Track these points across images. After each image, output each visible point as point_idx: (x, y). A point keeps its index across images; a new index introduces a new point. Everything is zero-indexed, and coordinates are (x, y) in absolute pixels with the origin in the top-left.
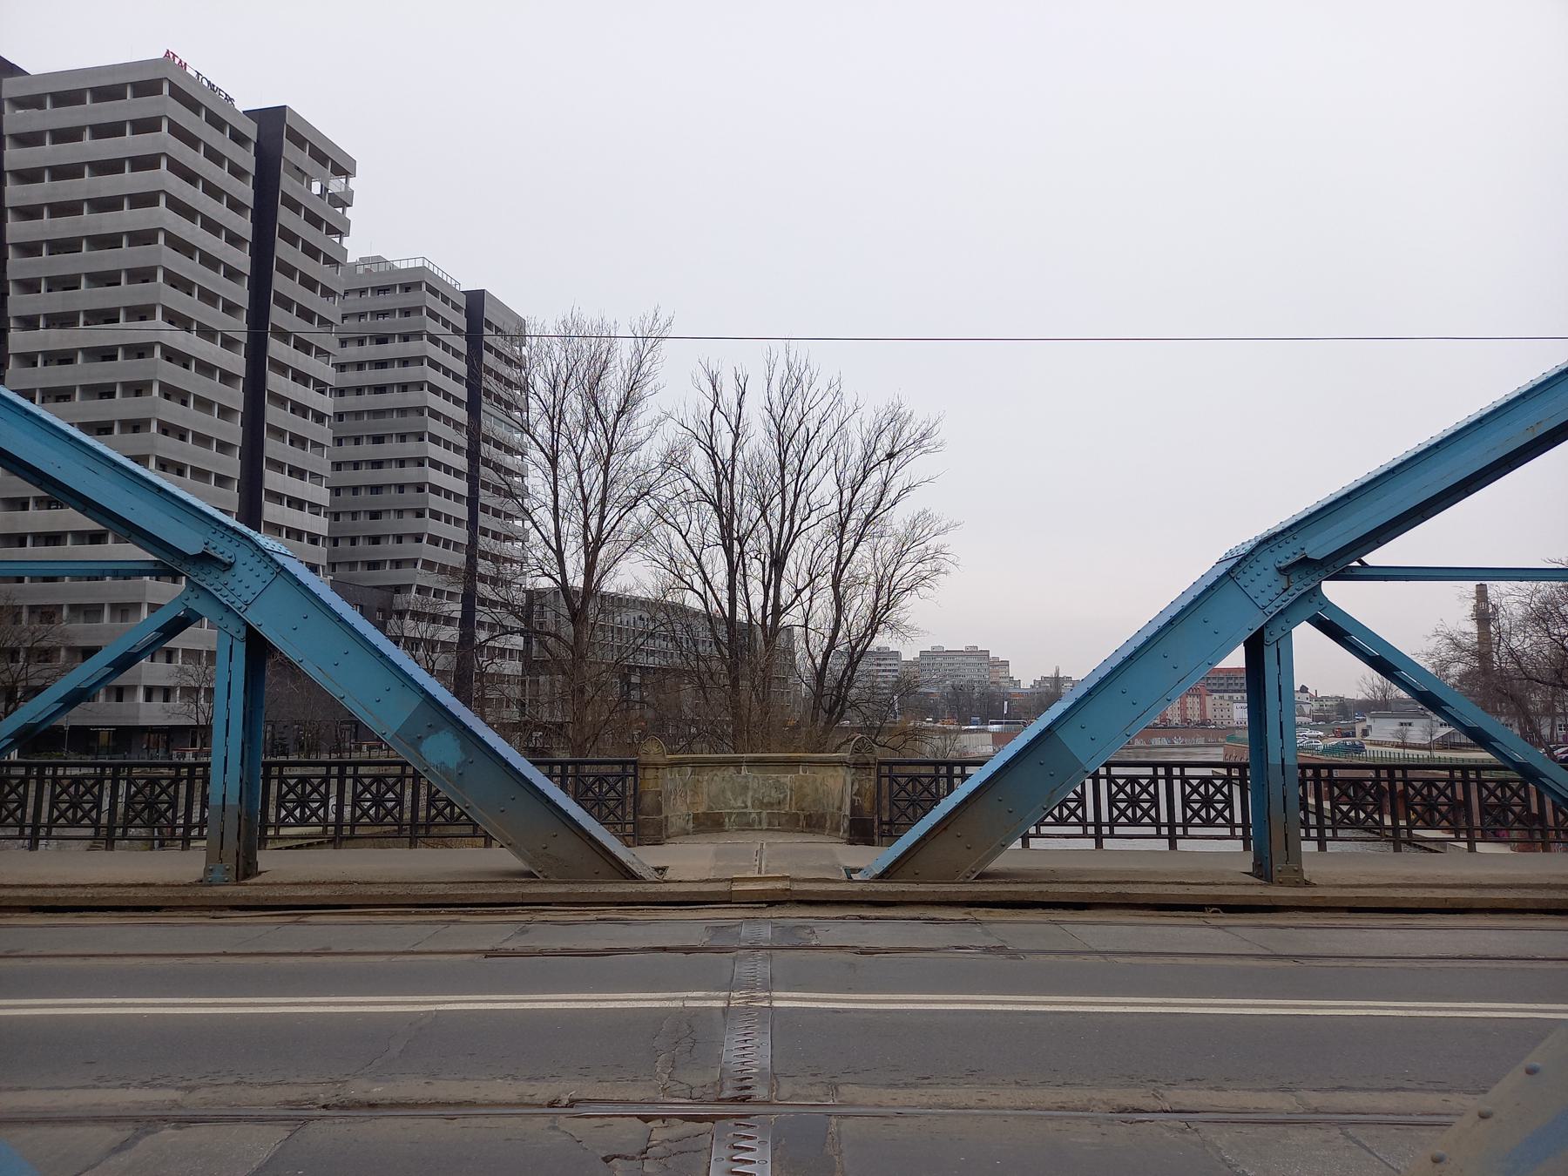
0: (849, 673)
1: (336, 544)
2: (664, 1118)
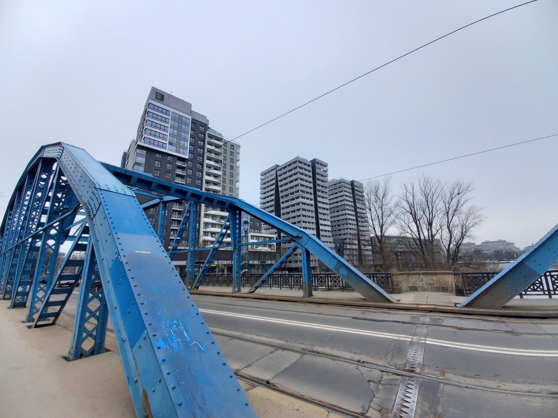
0: (457, 249)
2: (387, 372)
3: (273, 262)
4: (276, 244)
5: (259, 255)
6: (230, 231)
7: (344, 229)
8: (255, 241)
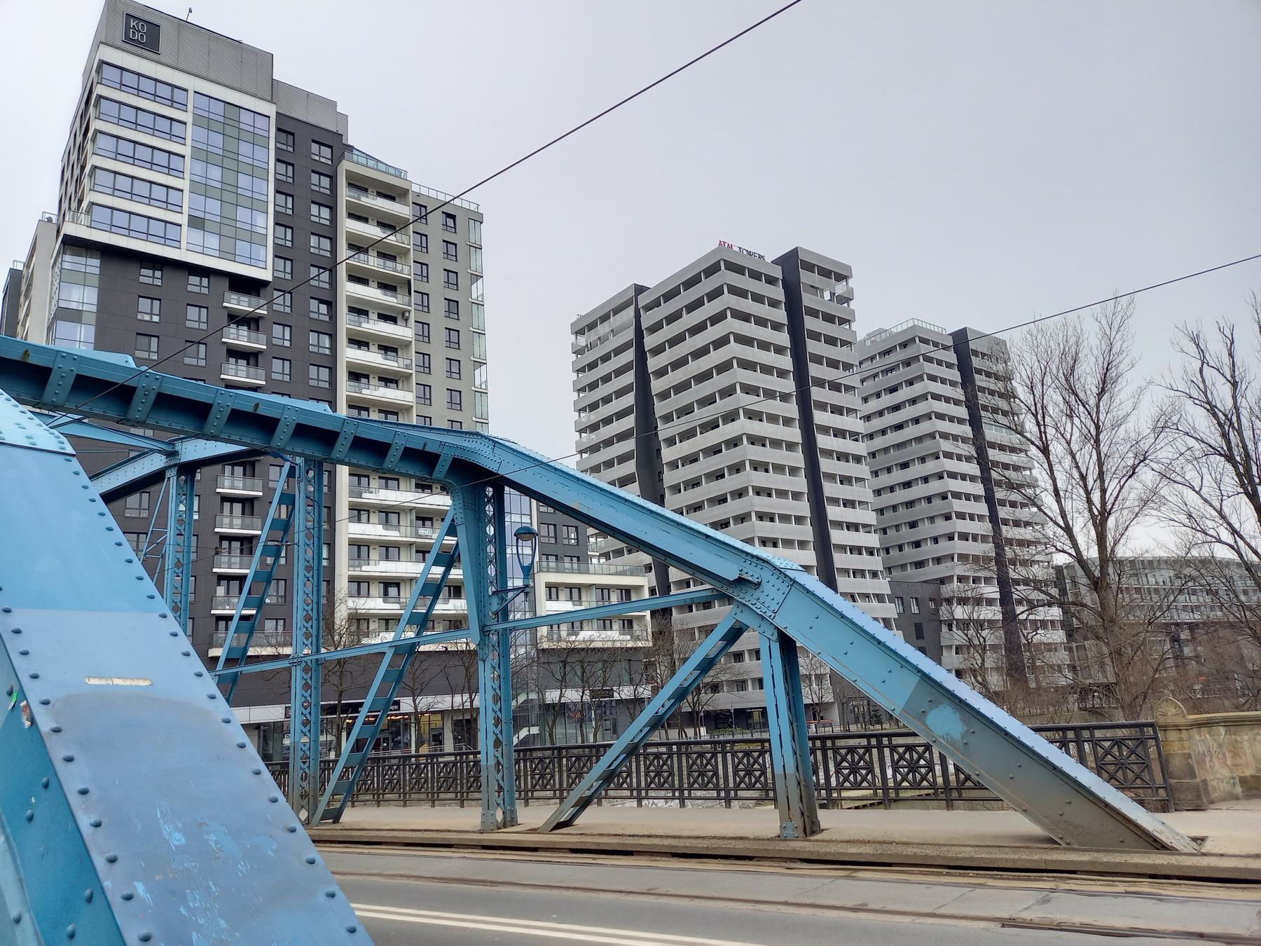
1: (888, 553)
3: (645, 691)
4: (653, 613)
5: (581, 662)
6: (460, 572)
7: (936, 540)
8: (563, 606)
